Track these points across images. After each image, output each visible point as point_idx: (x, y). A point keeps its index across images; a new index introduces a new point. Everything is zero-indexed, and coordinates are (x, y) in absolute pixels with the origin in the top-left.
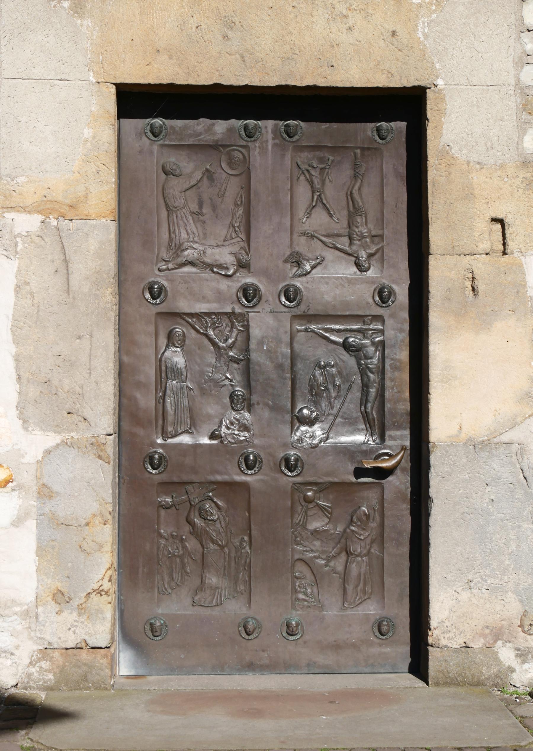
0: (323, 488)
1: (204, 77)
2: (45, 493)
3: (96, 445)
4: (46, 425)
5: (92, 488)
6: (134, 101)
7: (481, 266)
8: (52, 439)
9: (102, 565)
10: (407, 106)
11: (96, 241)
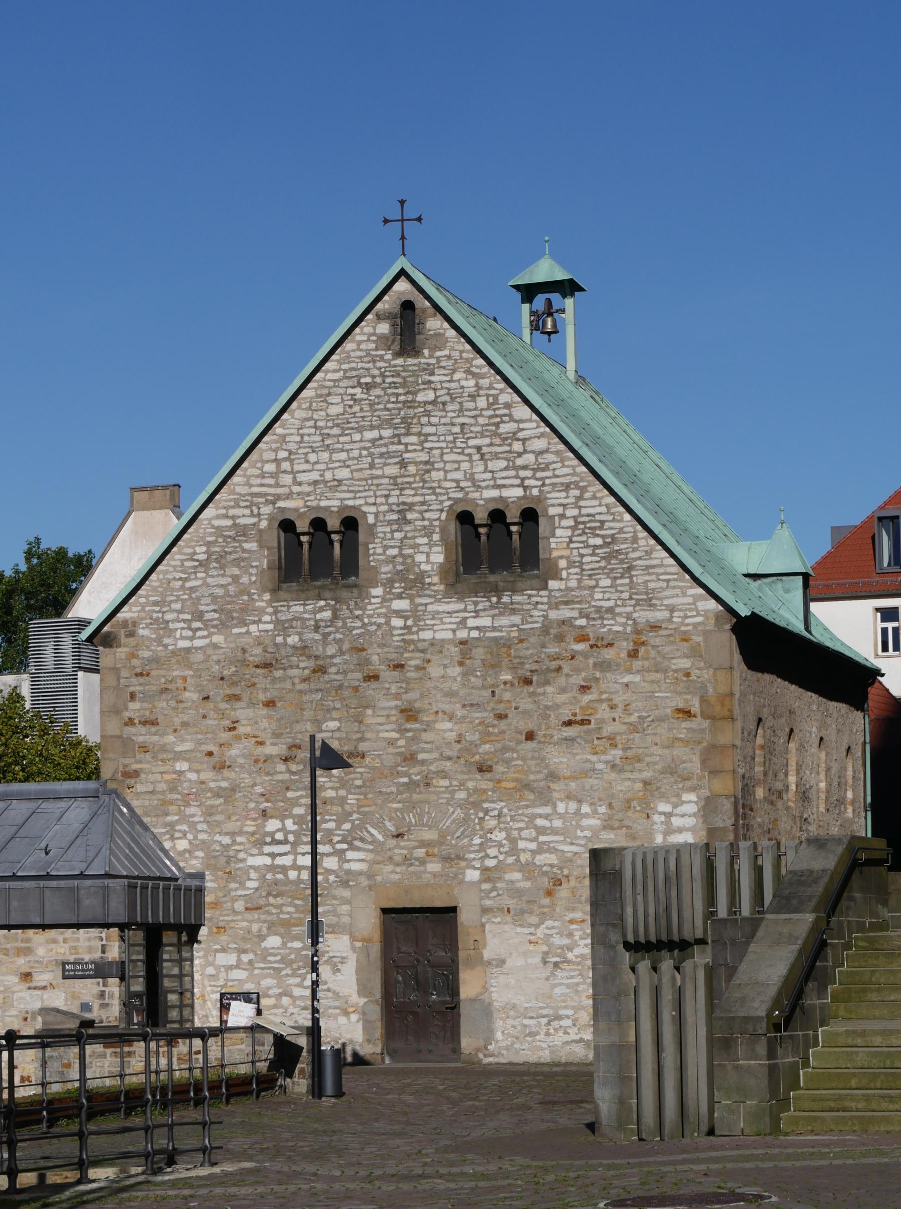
0: (437, 1012)
1: (401, 905)
2: (364, 1014)
3: (377, 1001)
4: (365, 996)
5: (376, 1012)
6: (385, 911)
7: (472, 952)
8: (366, 1000)
9: (378, 1033)
10: (453, 910)
11: (376, 948)
